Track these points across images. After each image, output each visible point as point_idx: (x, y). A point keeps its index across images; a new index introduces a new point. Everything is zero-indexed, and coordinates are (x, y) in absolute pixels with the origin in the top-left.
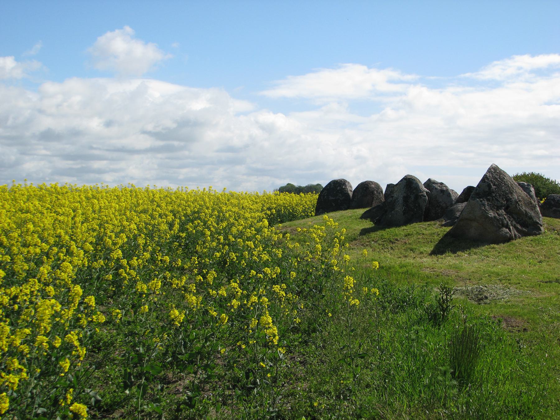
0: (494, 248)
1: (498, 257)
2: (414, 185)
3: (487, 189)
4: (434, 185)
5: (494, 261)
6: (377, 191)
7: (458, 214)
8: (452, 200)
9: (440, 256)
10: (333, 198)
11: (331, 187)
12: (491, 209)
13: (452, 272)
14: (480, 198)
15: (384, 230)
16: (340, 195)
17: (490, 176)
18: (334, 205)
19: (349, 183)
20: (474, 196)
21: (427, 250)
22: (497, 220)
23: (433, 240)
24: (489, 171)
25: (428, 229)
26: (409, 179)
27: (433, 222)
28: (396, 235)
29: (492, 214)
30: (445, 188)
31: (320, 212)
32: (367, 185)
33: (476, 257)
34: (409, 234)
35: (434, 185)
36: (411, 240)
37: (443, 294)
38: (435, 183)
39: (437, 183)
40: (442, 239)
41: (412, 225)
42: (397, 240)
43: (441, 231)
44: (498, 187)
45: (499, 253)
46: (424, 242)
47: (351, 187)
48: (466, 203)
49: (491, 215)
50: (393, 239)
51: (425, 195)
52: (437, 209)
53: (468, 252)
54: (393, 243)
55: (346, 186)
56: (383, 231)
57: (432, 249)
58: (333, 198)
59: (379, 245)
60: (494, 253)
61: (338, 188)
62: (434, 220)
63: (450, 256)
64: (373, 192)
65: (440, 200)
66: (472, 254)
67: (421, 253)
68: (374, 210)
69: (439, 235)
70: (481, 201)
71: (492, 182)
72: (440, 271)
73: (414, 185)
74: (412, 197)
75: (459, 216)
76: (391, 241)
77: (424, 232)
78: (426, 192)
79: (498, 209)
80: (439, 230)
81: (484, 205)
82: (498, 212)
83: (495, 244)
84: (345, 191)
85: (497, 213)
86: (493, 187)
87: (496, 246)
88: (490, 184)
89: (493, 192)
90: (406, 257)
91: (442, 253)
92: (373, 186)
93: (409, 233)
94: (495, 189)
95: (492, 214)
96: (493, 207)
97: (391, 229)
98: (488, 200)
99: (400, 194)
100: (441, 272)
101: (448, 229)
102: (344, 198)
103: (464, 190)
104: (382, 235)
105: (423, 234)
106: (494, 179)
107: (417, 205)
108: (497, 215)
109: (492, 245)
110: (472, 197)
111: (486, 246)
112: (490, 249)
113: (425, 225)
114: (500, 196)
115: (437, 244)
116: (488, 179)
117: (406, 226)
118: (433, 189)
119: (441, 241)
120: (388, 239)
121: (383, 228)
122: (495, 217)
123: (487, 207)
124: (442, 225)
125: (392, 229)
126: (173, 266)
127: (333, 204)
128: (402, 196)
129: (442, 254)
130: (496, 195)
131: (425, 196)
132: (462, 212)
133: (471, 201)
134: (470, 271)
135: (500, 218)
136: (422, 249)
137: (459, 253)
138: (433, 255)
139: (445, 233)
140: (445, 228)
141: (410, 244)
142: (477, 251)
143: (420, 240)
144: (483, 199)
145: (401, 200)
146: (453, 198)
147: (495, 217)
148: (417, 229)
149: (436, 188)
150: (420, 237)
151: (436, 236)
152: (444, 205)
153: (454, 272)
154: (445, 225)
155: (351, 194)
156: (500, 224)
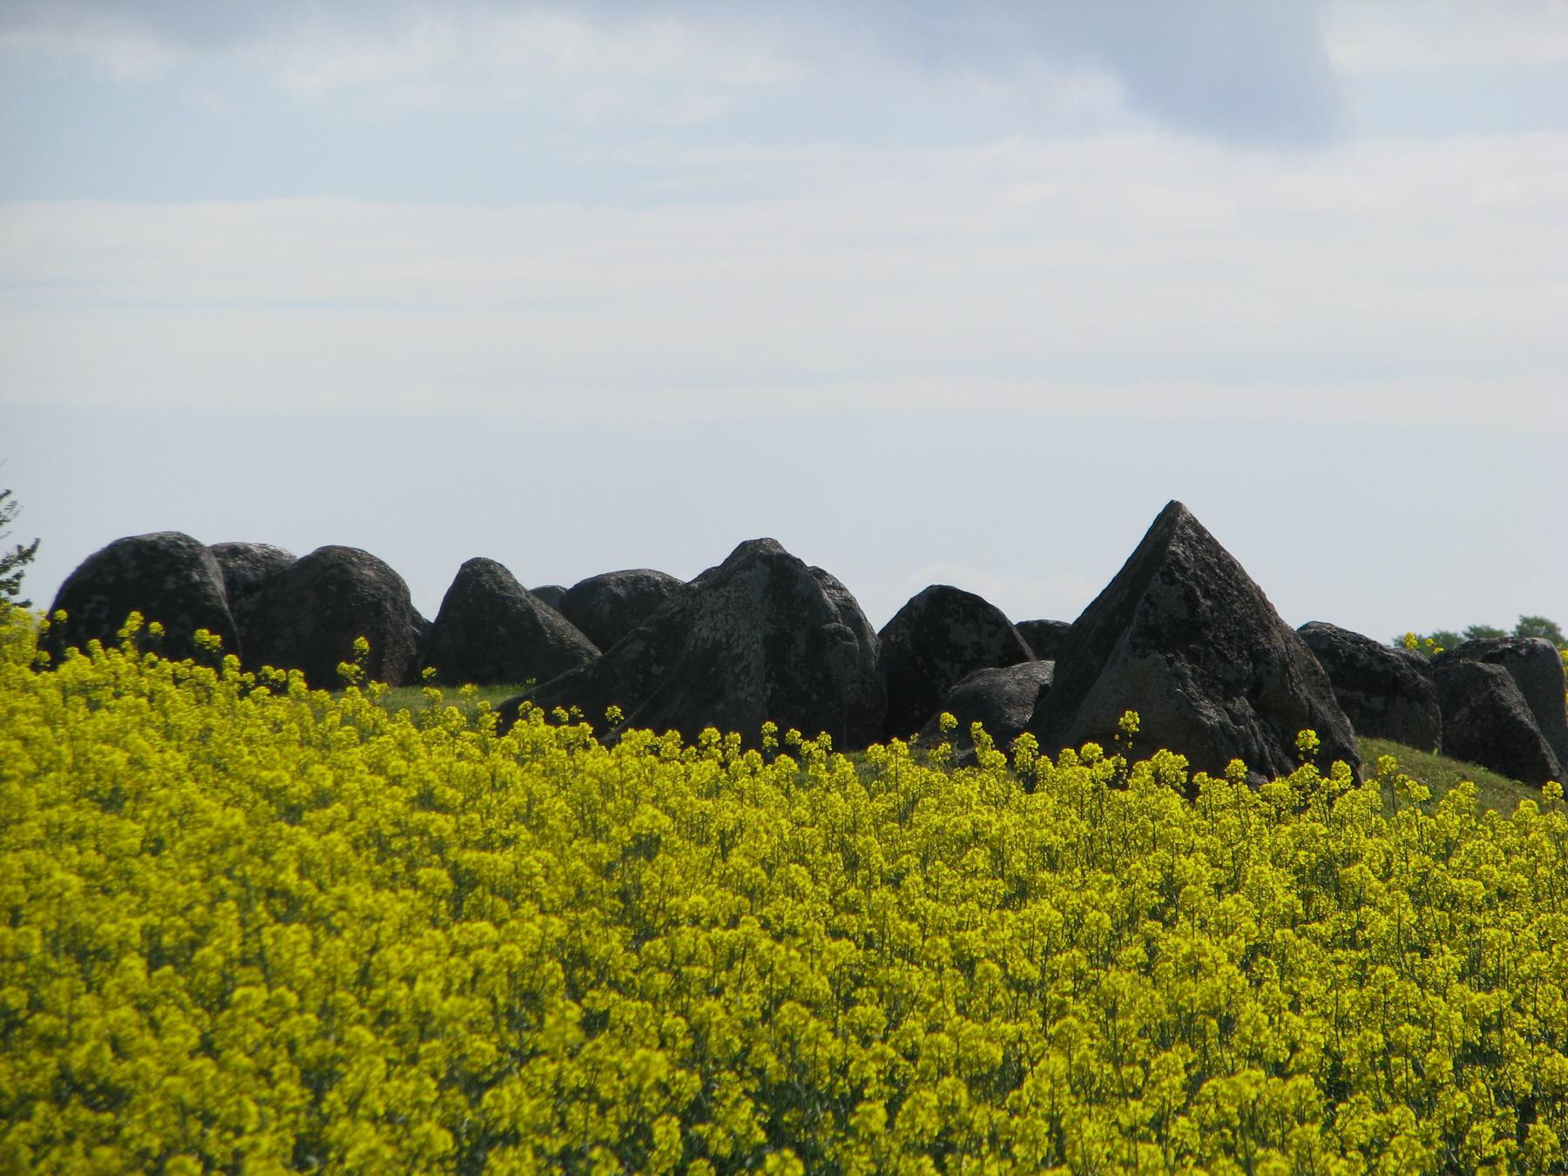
12: (1207, 695)
14: (1163, 648)
17: (1187, 559)
22: (1232, 738)
29: (1212, 713)
49: (1209, 718)
61: (170, 583)
71: (1198, 584)
79: (1228, 698)
81: (1180, 677)
85: (1228, 710)
88: (1193, 590)
89: (1207, 625)
95: (1212, 713)
96: (1212, 685)
98: (1193, 658)
106: (1202, 570)
107: (819, 675)
108: (1229, 721)
114: (1229, 639)
116: (1184, 570)
123: (1192, 688)
130: (1215, 637)
135: (1240, 732)
147: (1223, 726)
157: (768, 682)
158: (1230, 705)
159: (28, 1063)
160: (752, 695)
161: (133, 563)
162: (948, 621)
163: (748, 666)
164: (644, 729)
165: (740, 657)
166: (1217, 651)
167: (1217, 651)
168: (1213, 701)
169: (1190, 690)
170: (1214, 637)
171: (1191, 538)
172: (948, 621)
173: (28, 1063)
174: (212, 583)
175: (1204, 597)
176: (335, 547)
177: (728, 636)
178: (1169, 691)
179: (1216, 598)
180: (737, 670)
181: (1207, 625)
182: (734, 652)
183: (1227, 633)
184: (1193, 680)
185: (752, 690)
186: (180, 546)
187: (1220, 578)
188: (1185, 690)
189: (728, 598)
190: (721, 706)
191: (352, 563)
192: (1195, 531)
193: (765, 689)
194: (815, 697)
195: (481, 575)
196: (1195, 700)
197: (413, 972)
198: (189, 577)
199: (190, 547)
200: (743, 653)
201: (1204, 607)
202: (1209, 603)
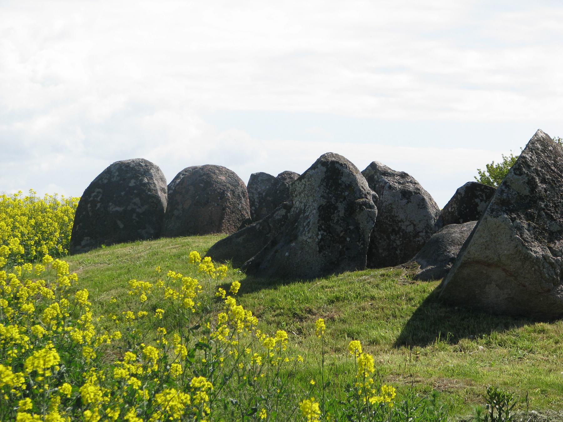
0: (543, 331)
1: (555, 351)
2: (344, 179)
3: (526, 191)
4: (386, 179)
5: (547, 361)
6: (233, 192)
7: (454, 251)
8: (428, 216)
9: (419, 349)
10: (118, 209)
11: (114, 180)
12: (537, 239)
13: (458, 383)
14: (509, 211)
15: (276, 289)
16: (137, 200)
17: (532, 160)
18: (122, 226)
19: (158, 169)
20: (495, 207)
21: (387, 335)
22: (551, 264)
23: (397, 313)
24: (531, 147)
25: (383, 285)
26: (333, 163)
27: (391, 270)
28: (307, 300)
29: (538, 249)
30: (411, 187)
31: (83, 243)
32: (208, 175)
33: (503, 351)
34: (338, 299)
35: (386, 179)
36: (347, 311)
37: (492, 408)
38: (386, 173)
39: (392, 174)
40: (419, 310)
41: (341, 276)
42: (310, 312)
43: (416, 291)
44: (552, 187)
45: (556, 343)
46: (377, 318)
47: (163, 179)
48: (473, 224)
49: (535, 252)
50: (300, 308)
51: (372, 202)
52: (392, 237)
53: (484, 341)
54: (301, 319)
55: (151, 178)
56: (272, 291)
57: (398, 333)
58: (118, 209)
59: (269, 323)
60: (546, 342)
61: (132, 183)
62: (394, 265)
63: (443, 349)
64: (222, 195)
65: (401, 216)
66: (494, 345)
67: (374, 342)
68: (240, 240)
69: (411, 299)
70: (513, 220)
71: (538, 175)
72: (429, 381)
73: (344, 179)
74: (341, 207)
75: (459, 255)
76: (295, 315)
77: (375, 292)
78: (374, 197)
79: (551, 240)
80: (408, 288)
81: (520, 229)
82: (552, 245)
83: (545, 321)
84: (150, 190)
85: (550, 248)
86: (542, 186)
87: (547, 326)
88: (533, 178)
89: (541, 199)
90: (338, 350)
91: (424, 342)
92: (223, 178)
93: (338, 294)
94: (546, 191)
95: (538, 249)
96: (541, 233)
97: (292, 286)
98: (530, 217)
99: (311, 199)
100: (431, 384)
101: (432, 286)
102: (146, 207)
103: (458, 192)
104: (272, 300)
105: (373, 298)
106: (542, 167)
107: (351, 227)
108: (550, 254)
109: (540, 325)
110: (492, 210)
111: (526, 326)
112: (536, 335)
113: (374, 276)
114: (556, 206)
115: (409, 321)
116: (529, 167)
117: (326, 278)
118: (383, 187)
119: (418, 315)
120: (289, 310)
121: (272, 284)
122: (545, 257)
123: (527, 234)
124: (416, 278)
125: (295, 287)
126: (209, 323)
127: (119, 222)
128: (316, 205)
129: (424, 345)
130: (546, 206)
131: (371, 207)
132: (465, 245)
133: (489, 218)
134: (499, 381)
135: (557, 261)
136: (374, 334)
137: (465, 342)
138: (403, 347)
139: (426, 295)
140: (425, 284)
141: (344, 321)
142: (505, 337)
143: (367, 312)
144: (518, 216)
145: (313, 214)
146: (432, 212)
147: (545, 257)
148: (357, 285)
149: (390, 187)
150: (367, 304)
151: (404, 303)
152: (410, 229)
153: (461, 384)
154: (424, 277)
155: (163, 197)
156: (556, 274)
157: (319, 230)
158: (552, 245)
159: (117, 391)
160: (310, 238)
161: (117, 173)
162: (477, 200)
163: (309, 222)
164: (223, 263)
165: (307, 217)
166: (546, 213)
167: (546, 213)
168: (541, 242)
169: (525, 236)
170: (545, 206)
171: (538, 149)
172: (477, 200)
173: (117, 391)
174: (154, 183)
175: (541, 182)
176: (208, 165)
177: (305, 206)
178: (511, 236)
179: (550, 183)
180: (305, 224)
181: (541, 199)
182: (306, 214)
183: (555, 204)
184: (529, 230)
185: (309, 235)
186: (141, 166)
187: (554, 171)
188: (521, 236)
189: (305, 185)
190: (293, 244)
191: (214, 173)
192: (541, 145)
193: (318, 235)
194: (348, 239)
195: (285, 179)
196: (528, 242)
197: (114, 396)
198: (142, 180)
199: (146, 166)
200: (309, 215)
201: (540, 188)
202: (544, 186)
